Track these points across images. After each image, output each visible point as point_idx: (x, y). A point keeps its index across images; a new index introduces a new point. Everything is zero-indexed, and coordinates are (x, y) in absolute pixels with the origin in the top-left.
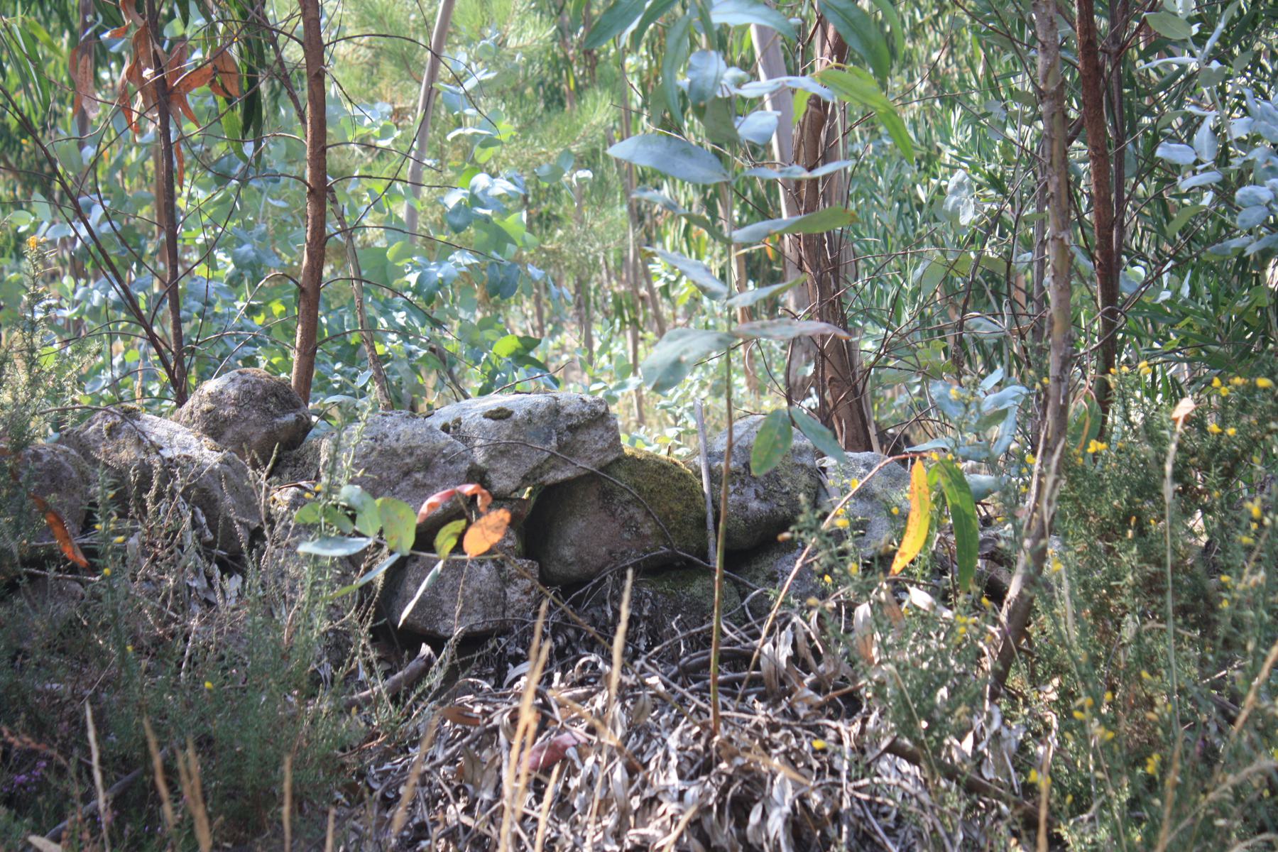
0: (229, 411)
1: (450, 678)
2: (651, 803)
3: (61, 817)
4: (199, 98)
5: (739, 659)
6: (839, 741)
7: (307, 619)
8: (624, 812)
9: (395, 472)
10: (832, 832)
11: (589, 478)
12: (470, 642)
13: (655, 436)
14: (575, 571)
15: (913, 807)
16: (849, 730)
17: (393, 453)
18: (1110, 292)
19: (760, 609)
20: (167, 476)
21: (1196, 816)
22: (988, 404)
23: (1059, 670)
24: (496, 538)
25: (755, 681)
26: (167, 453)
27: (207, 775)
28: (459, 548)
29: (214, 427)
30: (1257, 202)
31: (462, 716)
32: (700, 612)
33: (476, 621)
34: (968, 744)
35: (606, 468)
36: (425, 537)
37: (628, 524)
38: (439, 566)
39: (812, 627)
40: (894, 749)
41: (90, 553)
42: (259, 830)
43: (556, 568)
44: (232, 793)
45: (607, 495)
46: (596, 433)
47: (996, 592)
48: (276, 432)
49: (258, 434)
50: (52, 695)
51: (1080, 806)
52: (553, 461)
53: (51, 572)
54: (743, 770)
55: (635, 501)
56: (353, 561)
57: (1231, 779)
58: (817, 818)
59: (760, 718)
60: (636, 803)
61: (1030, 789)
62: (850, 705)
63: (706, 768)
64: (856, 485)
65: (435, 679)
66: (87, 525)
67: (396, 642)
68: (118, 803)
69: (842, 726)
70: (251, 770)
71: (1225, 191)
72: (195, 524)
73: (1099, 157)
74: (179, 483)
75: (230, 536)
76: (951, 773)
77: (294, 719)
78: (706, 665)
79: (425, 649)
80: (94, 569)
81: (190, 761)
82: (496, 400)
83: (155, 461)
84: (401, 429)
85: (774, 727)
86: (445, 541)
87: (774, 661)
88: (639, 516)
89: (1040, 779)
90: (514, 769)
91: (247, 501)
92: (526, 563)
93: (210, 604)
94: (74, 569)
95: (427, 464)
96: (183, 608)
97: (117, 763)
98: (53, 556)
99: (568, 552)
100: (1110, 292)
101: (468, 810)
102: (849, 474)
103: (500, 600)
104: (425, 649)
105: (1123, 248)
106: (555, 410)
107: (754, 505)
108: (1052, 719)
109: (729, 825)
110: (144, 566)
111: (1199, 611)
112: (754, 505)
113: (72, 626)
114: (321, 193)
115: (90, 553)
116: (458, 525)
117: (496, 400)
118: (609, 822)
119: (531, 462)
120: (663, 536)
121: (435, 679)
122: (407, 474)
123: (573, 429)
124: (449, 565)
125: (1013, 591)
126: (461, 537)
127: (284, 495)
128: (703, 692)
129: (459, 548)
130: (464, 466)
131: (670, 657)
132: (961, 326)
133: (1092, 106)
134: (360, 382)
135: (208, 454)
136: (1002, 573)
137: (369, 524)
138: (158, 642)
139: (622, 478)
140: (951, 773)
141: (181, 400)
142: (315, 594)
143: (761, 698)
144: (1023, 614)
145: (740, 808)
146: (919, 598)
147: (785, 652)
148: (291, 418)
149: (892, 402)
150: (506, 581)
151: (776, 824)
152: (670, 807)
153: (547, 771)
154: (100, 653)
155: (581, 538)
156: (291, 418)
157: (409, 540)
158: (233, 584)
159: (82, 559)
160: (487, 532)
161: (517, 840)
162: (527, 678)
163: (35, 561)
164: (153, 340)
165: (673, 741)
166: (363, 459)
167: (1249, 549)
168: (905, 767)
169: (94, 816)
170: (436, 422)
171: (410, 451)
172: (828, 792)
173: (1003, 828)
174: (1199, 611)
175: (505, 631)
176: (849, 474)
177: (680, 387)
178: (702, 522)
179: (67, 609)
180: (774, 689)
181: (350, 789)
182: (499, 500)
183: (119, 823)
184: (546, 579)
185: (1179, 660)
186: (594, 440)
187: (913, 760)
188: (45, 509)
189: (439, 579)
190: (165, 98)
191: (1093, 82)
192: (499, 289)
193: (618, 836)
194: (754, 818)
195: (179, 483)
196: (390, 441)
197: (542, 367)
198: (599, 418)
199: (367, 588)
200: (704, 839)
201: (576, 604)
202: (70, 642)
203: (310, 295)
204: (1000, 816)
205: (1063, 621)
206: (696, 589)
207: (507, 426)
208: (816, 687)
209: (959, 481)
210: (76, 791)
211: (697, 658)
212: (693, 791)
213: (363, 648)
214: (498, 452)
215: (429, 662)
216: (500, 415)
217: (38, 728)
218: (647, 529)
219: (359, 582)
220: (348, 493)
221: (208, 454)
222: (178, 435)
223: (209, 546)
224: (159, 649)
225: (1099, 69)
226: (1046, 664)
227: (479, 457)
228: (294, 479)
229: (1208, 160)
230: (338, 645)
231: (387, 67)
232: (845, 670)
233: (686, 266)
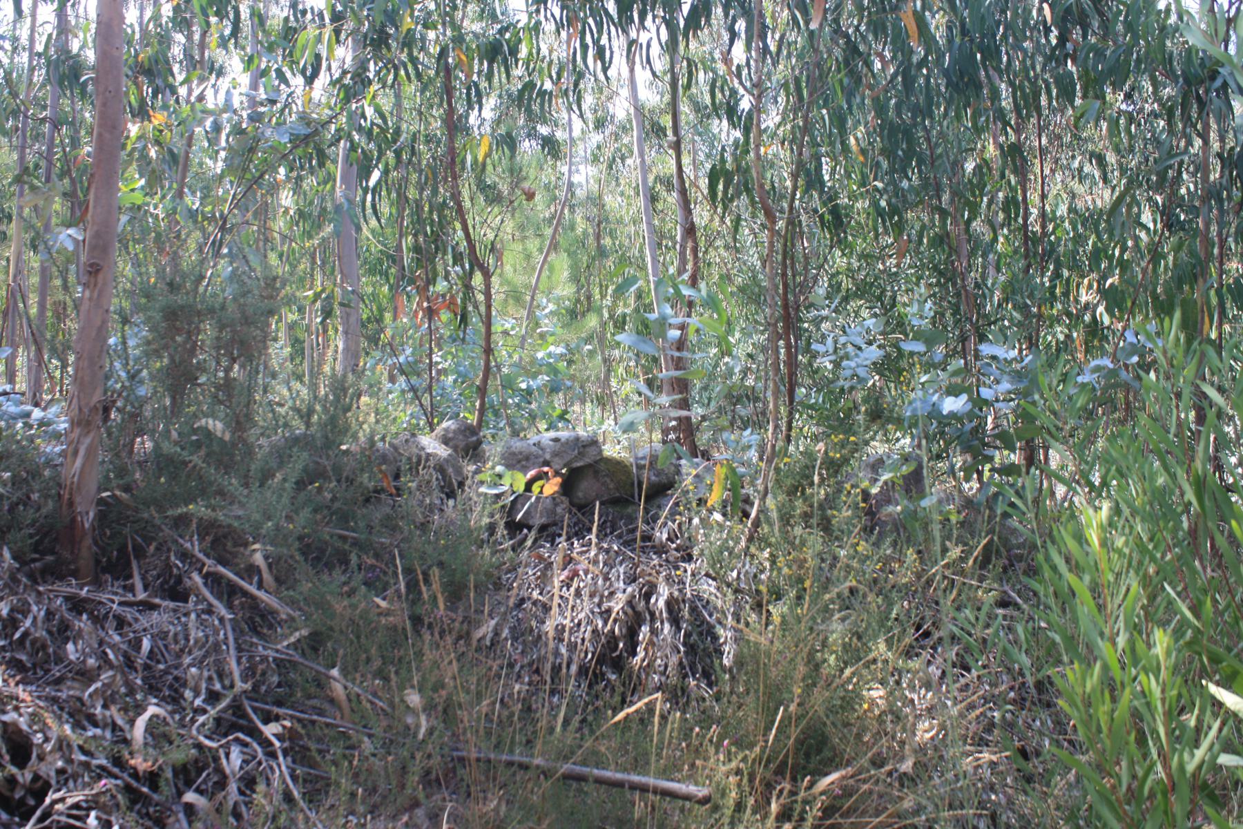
0: (451, 435)
1: (535, 541)
2: (612, 594)
3: (385, 590)
4: (445, 316)
5: (647, 538)
6: (686, 571)
7: (480, 519)
8: (602, 596)
9: (516, 461)
10: (682, 606)
11: (590, 466)
12: (543, 528)
13: (611, 451)
14: (583, 502)
15: (713, 598)
16: (690, 567)
17: (514, 454)
18: (792, 400)
19: (655, 519)
20: (427, 460)
21: (837, 59)
22: (745, 441)
23: (770, 545)
24: (556, 488)
25: (653, 547)
26: (429, 451)
27: (441, 577)
28: (541, 492)
29: (446, 441)
30: (850, 368)
31: (540, 557)
32: (632, 519)
33: (544, 520)
34: (735, 574)
35: (596, 462)
36: (528, 487)
37: (604, 484)
38: (533, 499)
39: (675, 526)
40: (707, 575)
41: (397, 489)
42: (460, 599)
43: (576, 501)
44: (451, 583)
45: (596, 472)
46: (593, 448)
47: (746, 515)
48: (469, 445)
49: (462, 445)
50: (382, 544)
51: (779, 598)
52: (576, 459)
53: (383, 496)
54: (648, 582)
55: (607, 475)
56: (498, 496)
57: (836, 590)
58: (677, 600)
59: (656, 562)
60: (606, 593)
61: (758, 591)
62: (689, 558)
63: (634, 581)
64: (694, 472)
65: (529, 543)
66: (397, 477)
67: (514, 527)
68: (408, 586)
69: (687, 565)
70: (458, 576)
71: (837, 365)
72: (437, 479)
73: (788, 346)
74: (431, 463)
75: (451, 484)
76: (729, 585)
77: (475, 555)
78: (635, 540)
79: (525, 531)
80: (399, 495)
81: (435, 572)
82: (552, 434)
83: (423, 453)
84: (517, 445)
85: (661, 566)
86: (536, 488)
87: (661, 539)
88: (608, 481)
89: (763, 588)
90: (558, 577)
91: (459, 471)
92: (563, 498)
93: (442, 510)
94: (391, 495)
95: (527, 458)
96: (431, 511)
97: (408, 571)
98: (383, 490)
99: (580, 494)
100: (792, 400)
101: (541, 594)
102: (689, 469)
103: (554, 512)
104: (525, 531)
105: (796, 383)
106: (577, 439)
107: (653, 478)
108: (767, 564)
109: (643, 603)
110: (416, 495)
111: (826, 526)
112: (653, 478)
113: (388, 517)
114: (488, 351)
115: (397, 489)
116: (540, 483)
117: (552, 434)
118: (596, 600)
119: (567, 458)
120: (617, 489)
121: (529, 543)
122: (519, 462)
123: (584, 446)
124: (538, 499)
125: (753, 515)
126: (542, 487)
127: (472, 468)
128: (633, 551)
129: (541, 492)
130: (541, 460)
131: (620, 537)
132: (733, 411)
133: (787, 328)
134: (501, 425)
135: (443, 452)
136: (747, 507)
137: (507, 481)
138: (422, 524)
139: (602, 466)
140: (729, 585)
141: (432, 430)
142: (484, 508)
143: (655, 553)
144: (757, 524)
145: (647, 597)
146: (717, 516)
147: (665, 536)
148: (474, 438)
149: (703, 439)
150: (556, 505)
151: (661, 603)
152: (619, 595)
153: (572, 579)
154: (400, 528)
155: (586, 488)
156: (474, 438)
157: (522, 488)
158: (451, 502)
159: (394, 491)
160: (551, 487)
161: (559, 605)
162: (562, 543)
163: (376, 491)
164: (421, 405)
165: (621, 570)
166: (503, 457)
167: (845, 503)
168: (710, 581)
169: (398, 591)
170: (531, 442)
171: (521, 453)
172: (680, 591)
173: (748, 607)
174: (826, 526)
175: (555, 524)
176: (689, 469)
177: (623, 432)
178: (633, 484)
179: (388, 510)
180: (660, 550)
181: (495, 584)
182: (557, 473)
183: (407, 595)
184: (572, 503)
185: (816, 541)
186: (592, 451)
187: (714, 579)
188: (381, 471)
189: (532, 505)
190: (431, 313)
191: (786, 318)
192: (554, 390)
193: (599, 605)
194: (653, 600)
195: (431, 463)
196: (513, 449)
197: (568, 421)
198: (593, 443)
199: (503, 507)
200: (633, 608)
201: (583, 514)
202: (390, 525)
203: (482, 391)
204: (747, 602)
205: (771, 530)
206: (629, 510)
207: (558, 445)
208: (677, 550)
209: (733, 470)
210: (392, 581)
211: (630, 537)
212: (629, 589)
213: (501, 531)
214: (556, 454)
215: (526, 536)
216: (556, 440)
217: (377, 556)
218: (611, 486)
219: (501, 504)
220: (499, 469)
221: (443, 452)
222: (431, 444)
223: (442, 487)
224: (424, 526)
225: (789, 314)
226: (764, 542)
227: (548, 457)
228: (475, 463)
229: (831, 350)
230: (492, 528)
231: (511, 301)
232: (688, 543)
233: (627, 386)
